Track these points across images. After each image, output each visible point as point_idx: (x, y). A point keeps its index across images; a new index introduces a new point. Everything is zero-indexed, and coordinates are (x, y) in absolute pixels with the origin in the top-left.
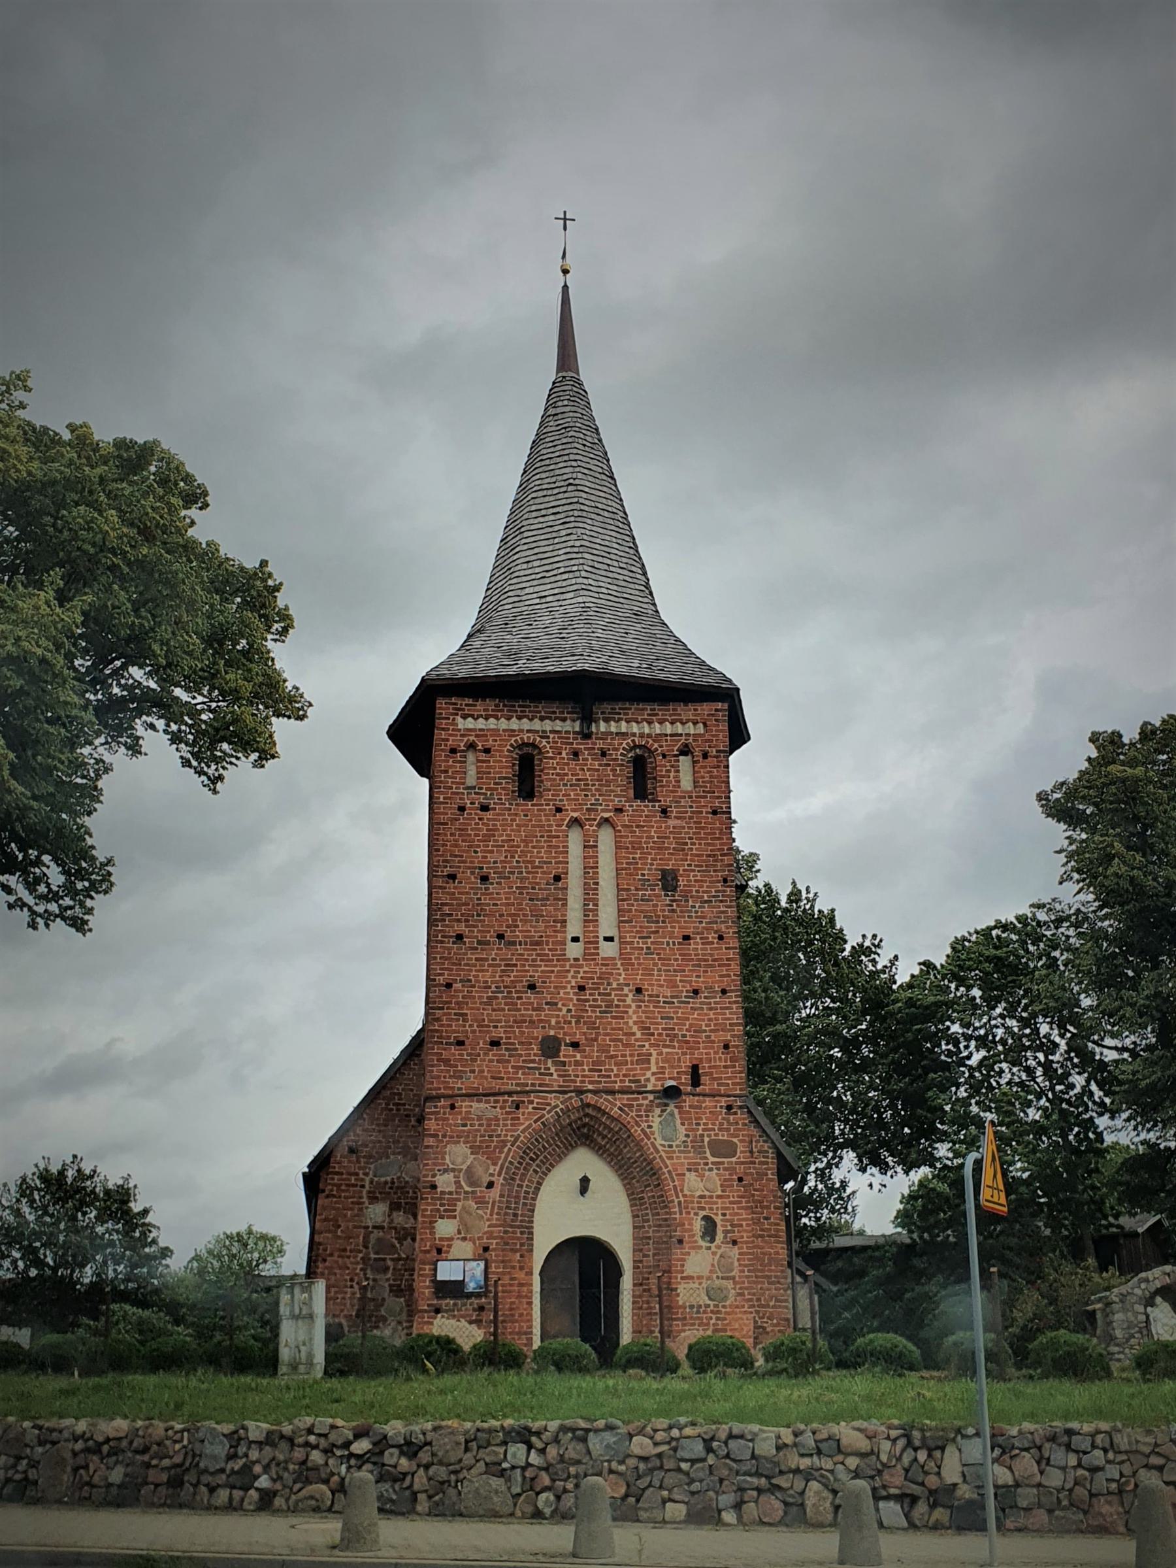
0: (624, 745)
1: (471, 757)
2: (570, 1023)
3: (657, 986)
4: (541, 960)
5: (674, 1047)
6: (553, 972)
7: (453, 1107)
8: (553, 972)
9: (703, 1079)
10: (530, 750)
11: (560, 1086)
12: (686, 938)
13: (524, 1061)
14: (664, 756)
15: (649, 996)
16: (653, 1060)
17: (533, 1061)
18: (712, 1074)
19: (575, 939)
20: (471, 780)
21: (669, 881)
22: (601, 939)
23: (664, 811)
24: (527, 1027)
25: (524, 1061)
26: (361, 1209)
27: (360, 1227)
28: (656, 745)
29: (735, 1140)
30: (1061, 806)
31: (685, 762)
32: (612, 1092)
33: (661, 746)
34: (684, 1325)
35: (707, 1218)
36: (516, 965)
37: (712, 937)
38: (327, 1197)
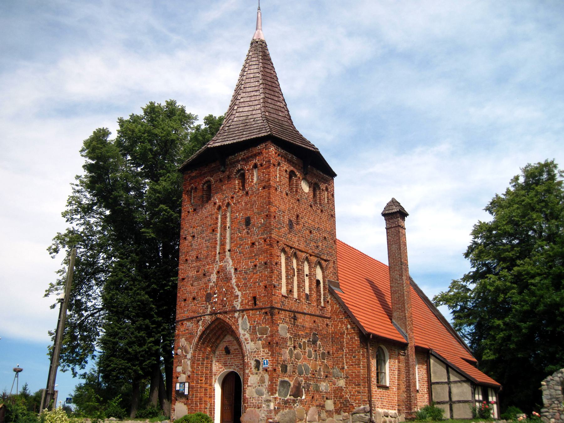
3: (242, 267)
9: (258, 302)
16: (239, 297)
17: (203, 304)
21: (248, 222)
23: (247, 193)
37: (262, 241)
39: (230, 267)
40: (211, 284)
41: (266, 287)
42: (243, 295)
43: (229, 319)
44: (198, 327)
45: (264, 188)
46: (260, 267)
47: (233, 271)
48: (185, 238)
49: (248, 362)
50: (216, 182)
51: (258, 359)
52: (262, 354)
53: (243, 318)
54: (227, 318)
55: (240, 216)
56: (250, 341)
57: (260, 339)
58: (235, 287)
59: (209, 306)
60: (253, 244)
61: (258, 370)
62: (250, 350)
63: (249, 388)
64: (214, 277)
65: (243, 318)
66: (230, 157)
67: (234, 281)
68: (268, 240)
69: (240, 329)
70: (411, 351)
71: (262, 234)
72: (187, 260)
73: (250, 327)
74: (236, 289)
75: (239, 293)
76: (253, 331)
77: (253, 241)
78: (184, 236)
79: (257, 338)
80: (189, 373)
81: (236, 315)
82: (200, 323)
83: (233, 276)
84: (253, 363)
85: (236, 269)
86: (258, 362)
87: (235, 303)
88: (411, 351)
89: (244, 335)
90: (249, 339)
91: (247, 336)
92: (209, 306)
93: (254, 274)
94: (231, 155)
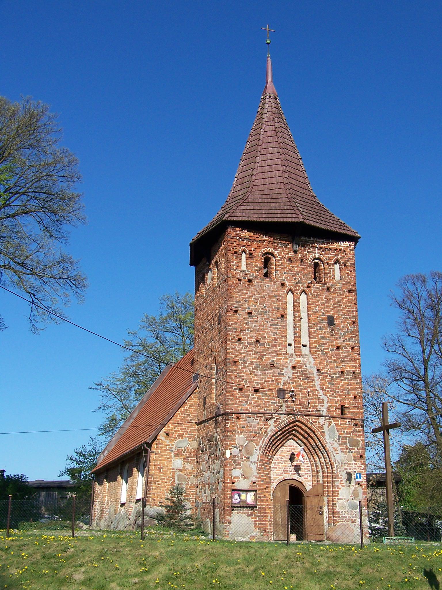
0: (311, 257)
1: (244, 256)
2: (290, 383)
3: (326, 369)
4: (277, 354)
5: (334, 397)
6: (281, 359)
7: (238, 418)
8: (281, 359)
9: (346, 411)
10: (317, 261)
11: (286, 412)
12: (338, 348)
13: (269, 399)
14: (328, 263)
15: (323, 373)
16: (325, 401)
17: (274, 400)
18: (240, 400)
19: (290, 345)
20: (244, 268)
21: (331, 321)
22: (293, 344)
23: (328, 289)
24: (270, 384)
25: (269, 399)
26: (171, 461)
27: (171, 469)
28: (324, 258)
29: (359, 439)
30: (191, 264)
31: (337, 266)
32: (309, 415)
33: (326, 259)
34: (339, 519)
35: (347, 473)
36: (265, 355)
37: (349, 348)
38: (156, 454)
39: (311, 365)
40: (286, 379)
41: (355, 397)
42: (331, 401)
43: (311, 423)
44: (267, 426)
45: (349, 291)
46: (347, 375)
47: (315, 371)
48: (236, 311)
49: (337, 473)
50: (283, 258)
51: (350, 471)
52: (354, 467)
53: (330, 425)
54: (310, 421)
55: (322, 313)
56: (339, 452)
57: (350, 451)
58: (319, 389)
59: (284, 405)
60: (338, 348)
61: (350, 483)
62: (339, 461)
63: (340, 501)
64: (288, 372)
65: (330, 425)
66: (302, 238)
67: (317, 382)
68: (356, 349)
69: (327, 437)
70: (295, 463)
71: (349, 340)
72: (239, 340)
73: (339, 437)
74: (321, 393)
75: (325, 398)
76: (343, 441)
77: (339, 345)
78: (234, 308)
79: (347, 449)
80: (254, 479)
81: (322, 420)
82: (271, 422)
83: (316, 378)
84: (344, 476)
85: (318, 370)
86: (349, 475)
87: (319, 407)
88: (295, 463)
89: (332, 444)
90: (339, 449)
91: (336, 445)
92: (284, 405)
93: (342, 380)
94: (305, 236)
